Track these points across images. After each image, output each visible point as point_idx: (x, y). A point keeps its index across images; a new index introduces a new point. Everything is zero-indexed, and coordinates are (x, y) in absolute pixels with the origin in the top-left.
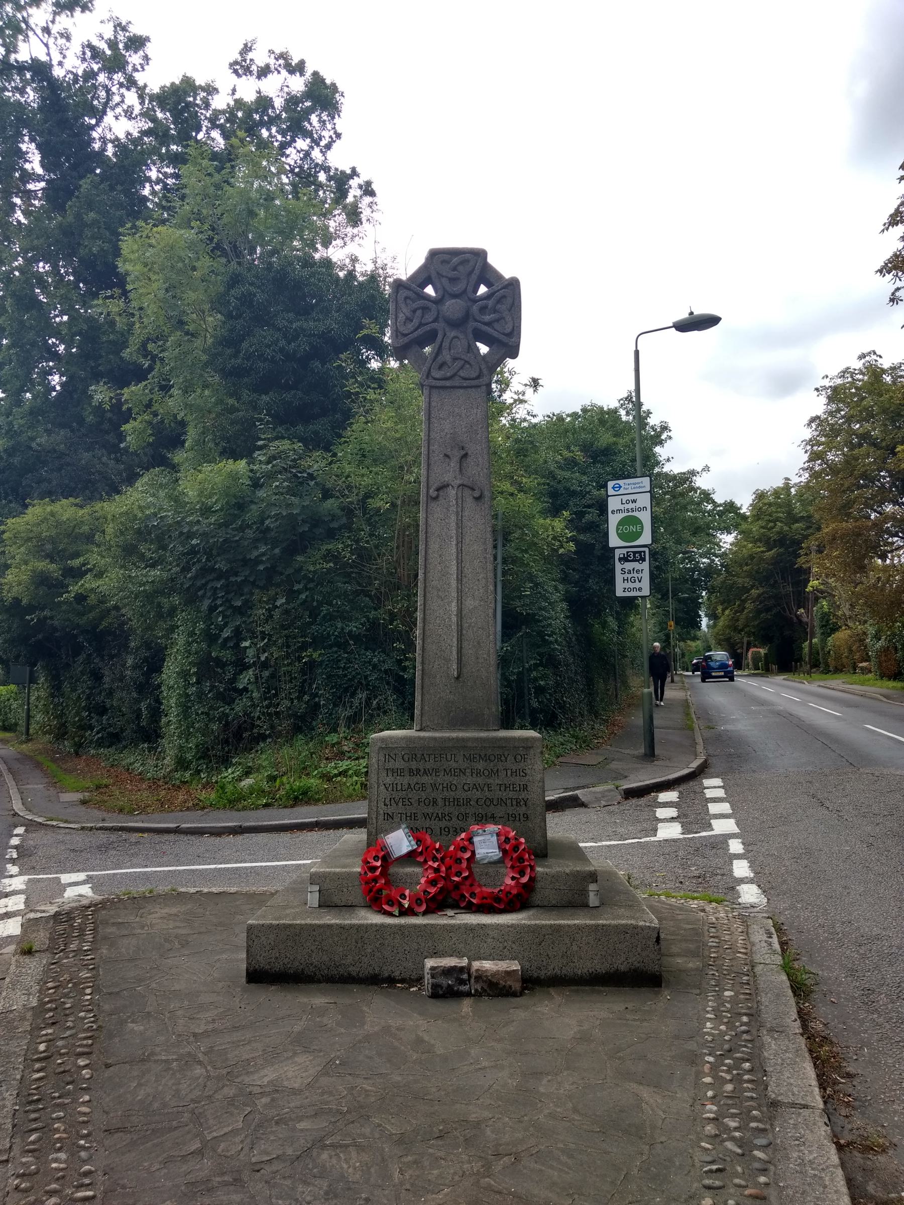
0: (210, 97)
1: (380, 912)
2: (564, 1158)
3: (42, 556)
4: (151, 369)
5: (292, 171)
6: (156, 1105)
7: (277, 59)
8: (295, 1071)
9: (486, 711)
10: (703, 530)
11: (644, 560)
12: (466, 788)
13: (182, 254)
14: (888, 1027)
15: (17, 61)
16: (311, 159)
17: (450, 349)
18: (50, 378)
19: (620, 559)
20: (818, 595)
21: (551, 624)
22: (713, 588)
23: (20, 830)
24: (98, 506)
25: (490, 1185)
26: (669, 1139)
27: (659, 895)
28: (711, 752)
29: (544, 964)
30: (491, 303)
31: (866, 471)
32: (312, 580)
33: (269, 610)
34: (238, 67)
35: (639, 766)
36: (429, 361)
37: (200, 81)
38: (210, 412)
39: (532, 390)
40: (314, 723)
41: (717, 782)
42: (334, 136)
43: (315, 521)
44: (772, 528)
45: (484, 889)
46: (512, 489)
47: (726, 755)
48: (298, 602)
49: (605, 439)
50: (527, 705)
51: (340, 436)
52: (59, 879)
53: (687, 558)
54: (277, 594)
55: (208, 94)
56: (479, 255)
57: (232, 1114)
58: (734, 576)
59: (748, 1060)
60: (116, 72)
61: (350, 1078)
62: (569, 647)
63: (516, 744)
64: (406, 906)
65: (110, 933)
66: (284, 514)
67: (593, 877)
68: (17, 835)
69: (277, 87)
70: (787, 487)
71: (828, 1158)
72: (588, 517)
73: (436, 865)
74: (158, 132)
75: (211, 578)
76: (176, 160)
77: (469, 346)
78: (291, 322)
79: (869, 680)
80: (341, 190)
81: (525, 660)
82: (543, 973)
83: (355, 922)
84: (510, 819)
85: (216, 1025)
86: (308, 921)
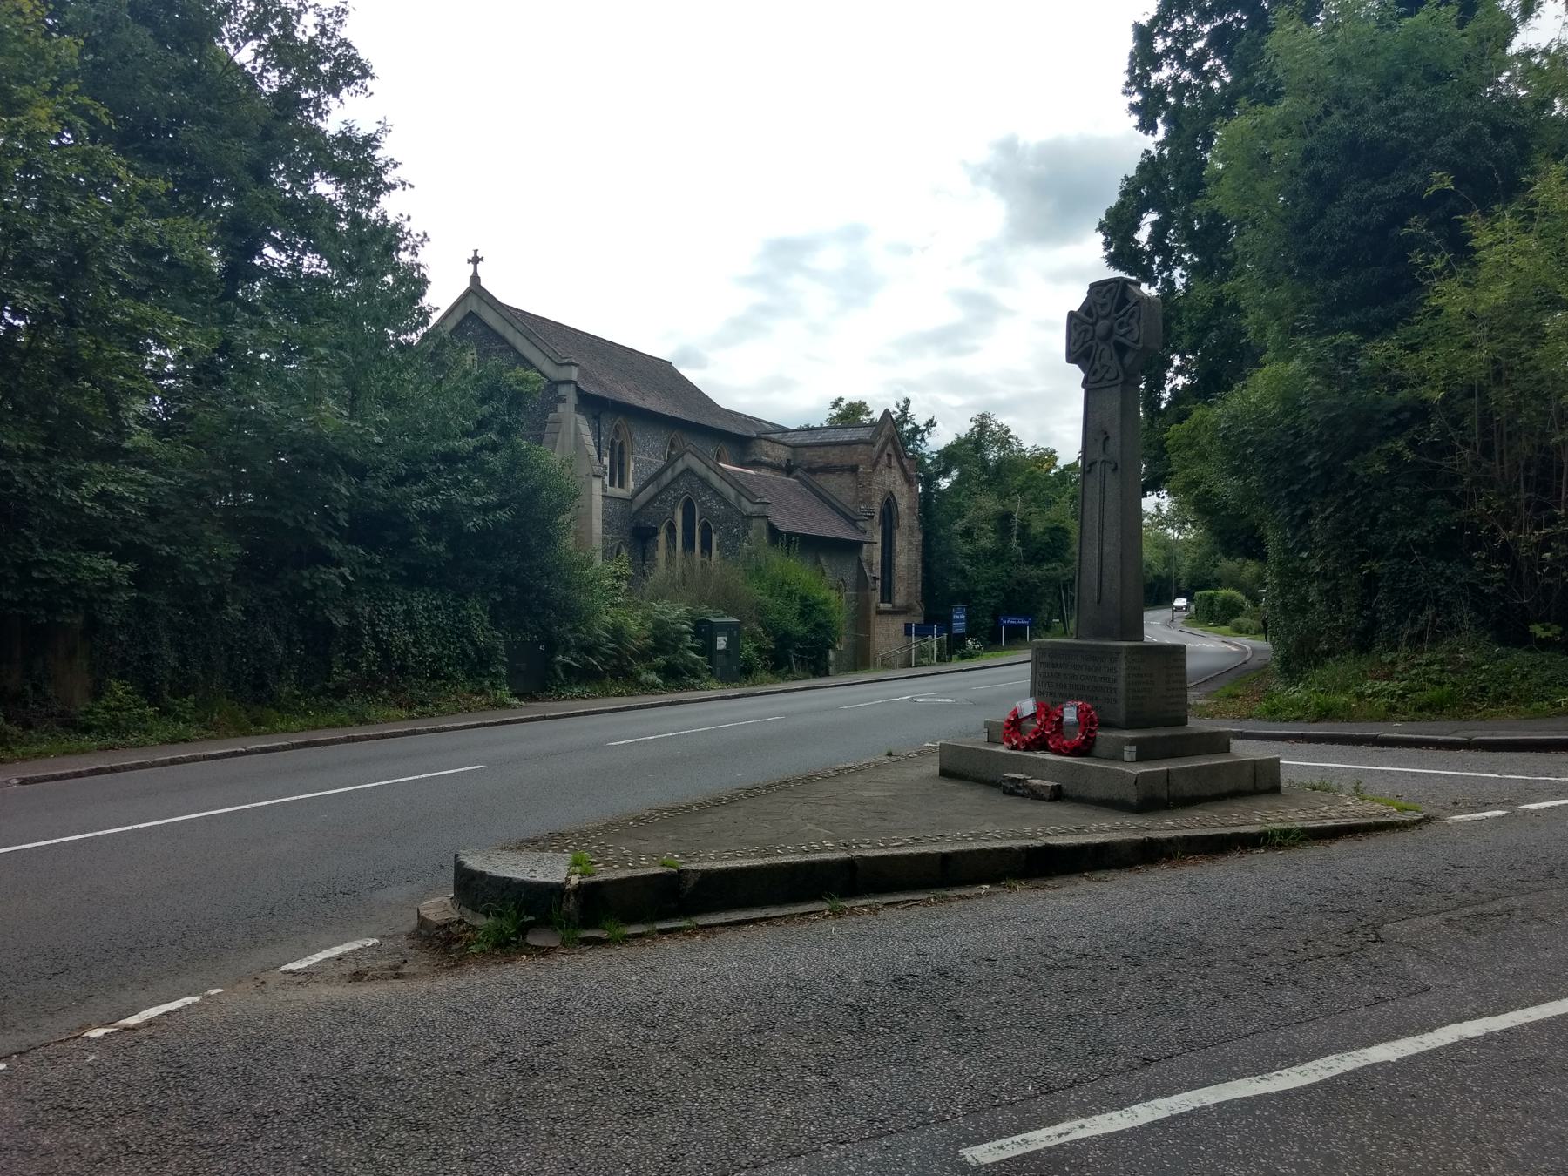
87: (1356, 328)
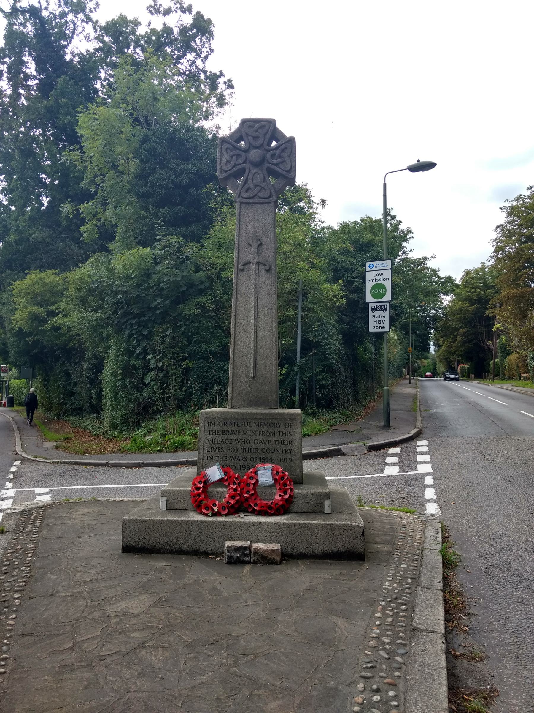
0: (136, 27)
1: (201, 513)
2: (283, 658)
3: (35, 304)
4: (96, 193)
5: (185, 74)
6: (53, 621)
7: (175, 4)
8: (137, 604)
9: (270, 398)
10: (432, 294)
11: (386, 310)
12: (256, 442)
13: (114, 123)
14: (498, 587)
15: (21, 7)
16: (196, 66)
17: (253, 180)
18: (41, 198)
19: (372, 309)
20: (500, 333)
21: (330, 348)
22: (437, 328)
23: (17, 463)
24: (69, 274)
25: (235, 672)
26: (347, 648)
27: (377, 508)
28: (425, 425)
29: (296, 546)
30: (278, 152)
31: (529, 258)
32: (188, 320)
33: (163, 337)
34: (152, 9)
35: (380, 432)
36: (240, 187)
37: (130, 18)
38: (130, 219)
39: (321, 206)
40: (189, 404)
41: (425, 442)
42: (209, 51)
43: (191, 285)
44: (474, 292)
45: (263, 502)
46: (307, 267)
47: (431, 426)
48: (180, 333)
49: (368, 236)
50: (314, 395)
51: (207, 234)
52: (34, 491)
53: (422, 310)
54: (168, 327)
55: (135, 26)
56: (271, 123)
57: (95, 627)
58: (450, 321)
59: (405, 604)
60: (79, 13)
61: (168, 608)
62: (342, 361)
63: (286, 417)
64: (216, 510)
65: (51, 523)
66: (171, 280)
67: (328, 496)
68: (15, 466)
69: (177, 21)
70: (483, 268)
71: (439, 663)
72: (355, 284)
73: (235, 487)
74: (106, 50)
75: (130, 318)
76: (114, 66)
77: (264, 178)
78: (178, 165)
79: (528, 384)
80: (214, 87)
81: (314, 369)
82: (295, 551)
83: (185, 519)
84: (281, 460)
85: (98, 577)
86: (159, 518)
87: (184, 236)
